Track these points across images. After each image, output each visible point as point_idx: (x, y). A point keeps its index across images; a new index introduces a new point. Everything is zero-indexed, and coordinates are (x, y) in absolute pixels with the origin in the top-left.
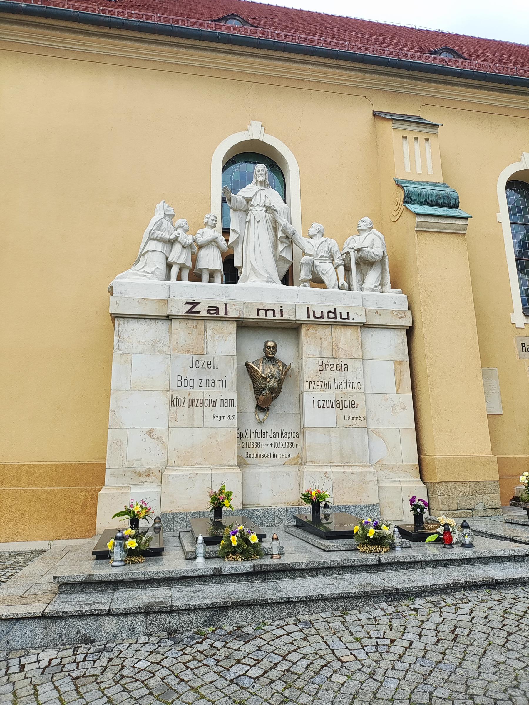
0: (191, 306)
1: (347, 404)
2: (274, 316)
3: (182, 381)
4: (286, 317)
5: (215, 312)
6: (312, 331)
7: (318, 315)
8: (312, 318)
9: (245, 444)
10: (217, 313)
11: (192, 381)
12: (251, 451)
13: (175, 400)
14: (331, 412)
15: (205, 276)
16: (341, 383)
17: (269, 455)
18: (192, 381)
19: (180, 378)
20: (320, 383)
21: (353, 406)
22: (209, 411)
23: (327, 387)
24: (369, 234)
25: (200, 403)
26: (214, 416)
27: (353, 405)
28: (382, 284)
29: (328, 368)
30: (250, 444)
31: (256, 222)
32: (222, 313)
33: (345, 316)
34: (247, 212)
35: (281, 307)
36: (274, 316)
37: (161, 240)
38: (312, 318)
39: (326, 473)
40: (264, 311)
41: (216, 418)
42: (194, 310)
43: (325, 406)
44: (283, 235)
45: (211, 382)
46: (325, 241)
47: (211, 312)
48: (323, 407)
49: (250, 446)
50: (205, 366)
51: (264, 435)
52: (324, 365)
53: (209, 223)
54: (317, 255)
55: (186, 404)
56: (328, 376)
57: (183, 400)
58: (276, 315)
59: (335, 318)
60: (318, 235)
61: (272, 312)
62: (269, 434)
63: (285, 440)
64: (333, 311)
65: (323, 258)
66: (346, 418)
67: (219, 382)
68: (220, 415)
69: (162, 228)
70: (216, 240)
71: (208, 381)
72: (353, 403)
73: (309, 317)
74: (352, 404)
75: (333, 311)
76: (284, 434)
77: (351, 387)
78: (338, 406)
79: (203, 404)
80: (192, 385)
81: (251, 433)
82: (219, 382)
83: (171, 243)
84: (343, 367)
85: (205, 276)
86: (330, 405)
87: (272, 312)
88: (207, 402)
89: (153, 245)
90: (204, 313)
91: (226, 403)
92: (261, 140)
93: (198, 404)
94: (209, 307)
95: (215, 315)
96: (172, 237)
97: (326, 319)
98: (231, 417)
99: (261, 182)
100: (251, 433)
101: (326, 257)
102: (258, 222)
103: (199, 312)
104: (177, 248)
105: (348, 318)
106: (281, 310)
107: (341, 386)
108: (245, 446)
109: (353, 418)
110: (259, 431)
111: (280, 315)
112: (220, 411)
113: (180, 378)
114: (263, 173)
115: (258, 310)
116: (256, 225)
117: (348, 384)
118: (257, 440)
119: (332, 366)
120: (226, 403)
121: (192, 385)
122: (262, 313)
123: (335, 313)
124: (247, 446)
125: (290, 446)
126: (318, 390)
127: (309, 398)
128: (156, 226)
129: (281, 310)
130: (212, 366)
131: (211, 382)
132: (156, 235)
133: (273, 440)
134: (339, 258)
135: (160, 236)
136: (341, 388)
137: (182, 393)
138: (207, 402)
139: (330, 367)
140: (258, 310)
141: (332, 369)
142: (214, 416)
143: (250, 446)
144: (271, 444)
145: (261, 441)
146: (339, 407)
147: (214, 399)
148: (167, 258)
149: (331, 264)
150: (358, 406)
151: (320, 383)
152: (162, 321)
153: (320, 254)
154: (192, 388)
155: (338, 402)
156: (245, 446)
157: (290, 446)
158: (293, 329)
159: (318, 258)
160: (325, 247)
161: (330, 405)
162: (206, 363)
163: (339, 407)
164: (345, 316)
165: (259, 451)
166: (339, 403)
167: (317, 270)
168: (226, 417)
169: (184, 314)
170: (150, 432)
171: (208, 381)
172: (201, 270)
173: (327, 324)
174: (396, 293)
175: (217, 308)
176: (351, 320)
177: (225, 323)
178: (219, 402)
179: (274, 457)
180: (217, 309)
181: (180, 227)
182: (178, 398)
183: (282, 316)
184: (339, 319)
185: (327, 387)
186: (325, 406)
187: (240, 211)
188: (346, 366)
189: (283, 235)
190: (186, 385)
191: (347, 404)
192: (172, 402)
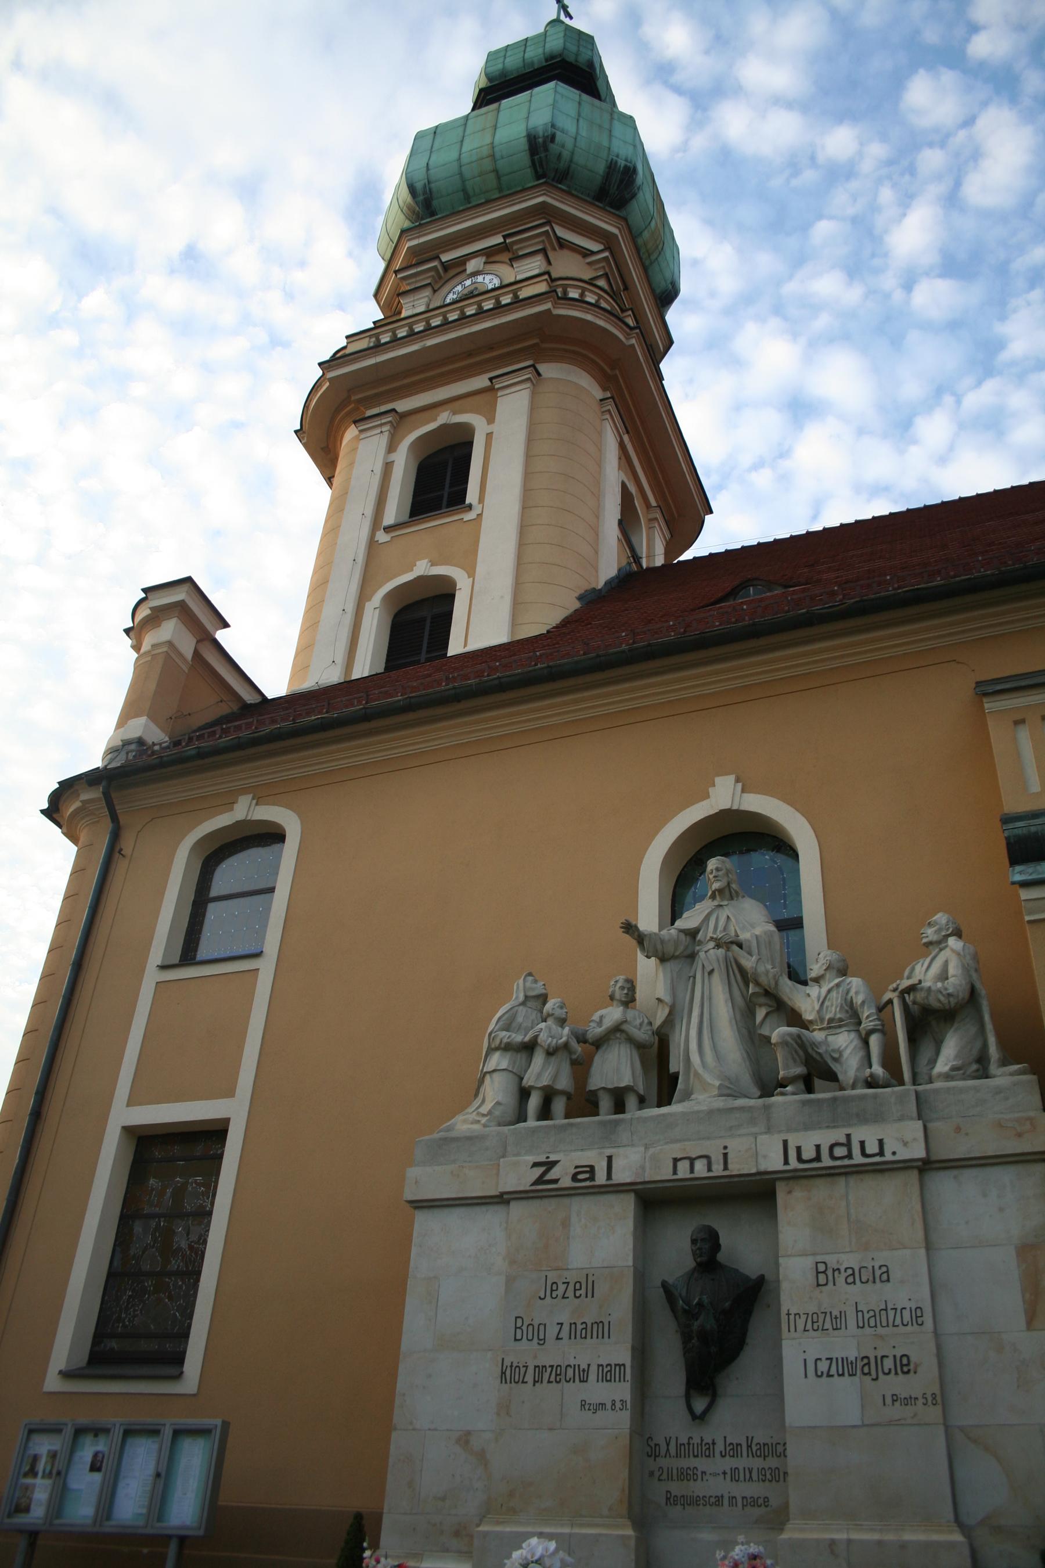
0: (543, 1169)
1: (888, 1364)
2: (709, 1170)
3: (524, 1328)
4: (735, 1168)
5: (587, 1175)
6: (798, 1194)
7: (808, 1153)
8: (794, 1164)
9: (665, 1473)
10: (592, 1178)
11: (542, 1328)
12: (676, 1488)
13: (509, 1369)
14: (847, 1388)
15: (605, 1103)
16: (872, 1313)
17: (719, 1500)
18: (542, 1328)
19: (519, 1321)
20: (821, 1317)
21: (905, 1369)
22: (575, 1392)
23: (838, 1322)
24: (941, 950)
25: (556, 1375)
26: (583, 1404)
27: (904, 1366)
28: (982, 1059)
29: (841, 1279)
30: (675, 1471)
31: (706, 974)
32: (601, 1178)
33: (872, 1148)
34: (692, 956)
35: (725, 1148)
36: (709, 1170)
37: (507, 1048)
38: (794, 1164)
39: (833, 1543)
40: (687, 1163)
41: (587, 1407)
42: (548, 1177)
43: (833, 1371)
44: (757, 990)
45: (580, 1327)
46: (838, 985)
47: (580, 1177)
48: (829, 1375)
49: (675, 1477)
50: (570, 1293)
51: (708, 1450)
52: (830, 1273)
53: (617, 996)
54: (822, 1020)
55: (529, 1378)
56: (846, 1296)
57: (523, 1370)
58: (714, 1167)
59: (850, 1156)
60: (828, 976)
61: (704, 1161)
62: (720, 1447)
63: (757, 1463)
64: (843, 1140)
65: (833, 1025)
66: (889, 1400)
67: (595, 1326)
68: (595, 1399)
69: (514, 1025)
70: (624, 1027)
71: (573, 1326)
72: (905, 1361)
73: (786, 1162)
74: (902, 1365)
75: (843, 1140)
76: (754, 1448)
77: (898, 1321)
78: (866, 1370)
79: (563, 1377)
80: (542, 1337)
81: (679, 1446)
82: (595, 1326)
83: (529, 1048)
84: (878, 1273)
85: (605, 1103)
86: (847, 1368)
87: (704, 1161)
88: (570, 1371)
89: (498, 1061)
90: (566, 1182)
91: (609, 1373)
92: (735, 807)
93: (552, 1378)
94: (576, 1167)
95: (588, 1183)
96: (527, 1039)
97: (826, 1161)
98: (618, 1405)
99: (720, 891)
100: (679, 1446)
101: (841, 1020)
102: (711, 972)
103: (556, 1181)
104: (539, 1059)
105: (881, 1153)
106: (725, 1155)
107: (873, 1319)
108: (664, 1476)
109: (909, 1401)
110: (696, 1440)
111: (722, 1167)
112: (597, 1391)
113: (519, 1321)
114: (720, 873)
115: (676, 1161)
116: (706, 981)
117: (891, 1313)
118: (693, 1462)
119: (850, 1272)
120: (609, 1373)
121: (542, 1337)
122: (683, 1168)
123: (848, 1144)
124: (670, 1478)
125: (768, 1476)
126: (815, 1334)
127: (797, 1350)
128: (501, 1023)
129: (725, 1155)
130: (583, 1292)
131: (580, 1327)
132: (497, 1042)
133: (729, 1463)
134: (868, 1017)
135: (505, 1040)
136: (872, 1324)
137: (527, 1353)
138: (570, 1371)
139: (844, 1275)
140: (676, 1161)
141: (850, 1280)
142: (583, 1404)
143: (675, 1477)
144: (724, 1473)
145: (700, 1464)
146: (869, 1373)
147: (584, 1366)
148: (522, 1079)
149: (853, 1035)
150: (919, 1370)
151: (821, 1317)
152: (492, 1208)
153: (827, 1017)
154: (542, 1342)
155: (865, 1361)
156: (664, 1476)
157: (768, 1476)
158: (757, 1194)
159: (825, 1025)
160: (836, 998)
161: (847, 1368)
162: (571, 1287)
163: (869, 1373)
164: (872, 1148)
165: (699, 1488)
166: (869, 1364)
167: (820, 1054)
168: (609, 1406)
169: (528, 1188)
170: (464, 1439)
171: (573, 1326)
172: (594, 1093)
173: (830, 1174)
174: (1011, 1074)
175: (592, 1167)
176: (888, 1157)
177: (611, 1198)
178: (594, 1369)
179: (730, 1504)
180: (592, 1169)
181: (549, 1015)
182: (515, 1365)
183: (726, 1168)
184: (858, 1159)
185: (838, 1322)
186: (833, 1371)
187: (673, 957)
188: (884, 1269)
189: (757, 990)
190: (530, 1337)
191: (888, 1364)
192: (503, 1373)
